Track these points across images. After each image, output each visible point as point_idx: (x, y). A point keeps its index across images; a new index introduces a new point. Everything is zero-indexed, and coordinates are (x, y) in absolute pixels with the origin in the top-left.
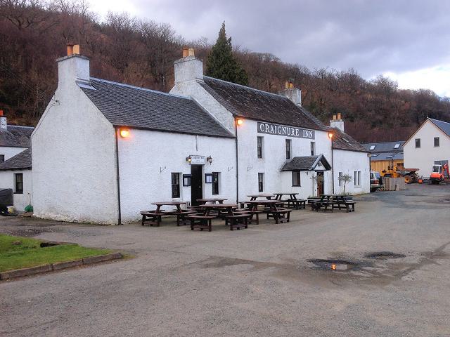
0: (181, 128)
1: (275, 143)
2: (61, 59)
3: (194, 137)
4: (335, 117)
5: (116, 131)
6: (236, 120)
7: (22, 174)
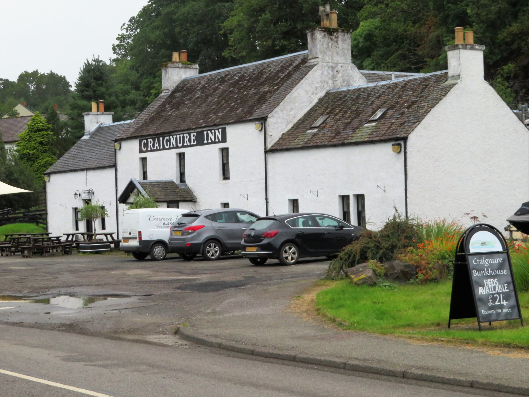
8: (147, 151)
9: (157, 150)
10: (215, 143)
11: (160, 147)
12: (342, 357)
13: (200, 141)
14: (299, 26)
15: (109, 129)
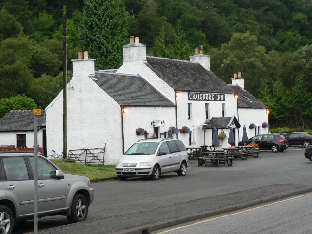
0: (153, 103)
1: (198, 106)
2: (76, 60)
3: (155, 108)
4: (235, 75)
5: (122, 109)
6: (176, 93)
7: (25, 134)
8: (192, 100)
9: (197, 100)
10: (221, 101)
12: (294, 81)
13: (215, 100)
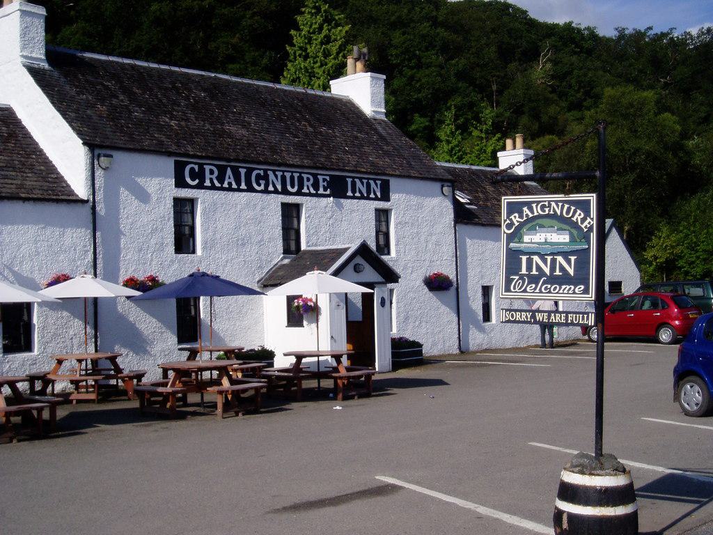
11: (239, 183)
13: (338, 189)
14: (628, 193)
15: (329, 121)
